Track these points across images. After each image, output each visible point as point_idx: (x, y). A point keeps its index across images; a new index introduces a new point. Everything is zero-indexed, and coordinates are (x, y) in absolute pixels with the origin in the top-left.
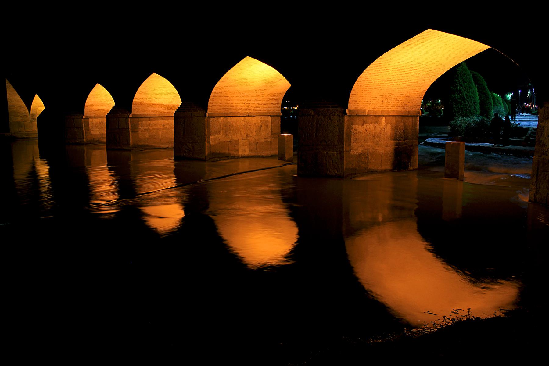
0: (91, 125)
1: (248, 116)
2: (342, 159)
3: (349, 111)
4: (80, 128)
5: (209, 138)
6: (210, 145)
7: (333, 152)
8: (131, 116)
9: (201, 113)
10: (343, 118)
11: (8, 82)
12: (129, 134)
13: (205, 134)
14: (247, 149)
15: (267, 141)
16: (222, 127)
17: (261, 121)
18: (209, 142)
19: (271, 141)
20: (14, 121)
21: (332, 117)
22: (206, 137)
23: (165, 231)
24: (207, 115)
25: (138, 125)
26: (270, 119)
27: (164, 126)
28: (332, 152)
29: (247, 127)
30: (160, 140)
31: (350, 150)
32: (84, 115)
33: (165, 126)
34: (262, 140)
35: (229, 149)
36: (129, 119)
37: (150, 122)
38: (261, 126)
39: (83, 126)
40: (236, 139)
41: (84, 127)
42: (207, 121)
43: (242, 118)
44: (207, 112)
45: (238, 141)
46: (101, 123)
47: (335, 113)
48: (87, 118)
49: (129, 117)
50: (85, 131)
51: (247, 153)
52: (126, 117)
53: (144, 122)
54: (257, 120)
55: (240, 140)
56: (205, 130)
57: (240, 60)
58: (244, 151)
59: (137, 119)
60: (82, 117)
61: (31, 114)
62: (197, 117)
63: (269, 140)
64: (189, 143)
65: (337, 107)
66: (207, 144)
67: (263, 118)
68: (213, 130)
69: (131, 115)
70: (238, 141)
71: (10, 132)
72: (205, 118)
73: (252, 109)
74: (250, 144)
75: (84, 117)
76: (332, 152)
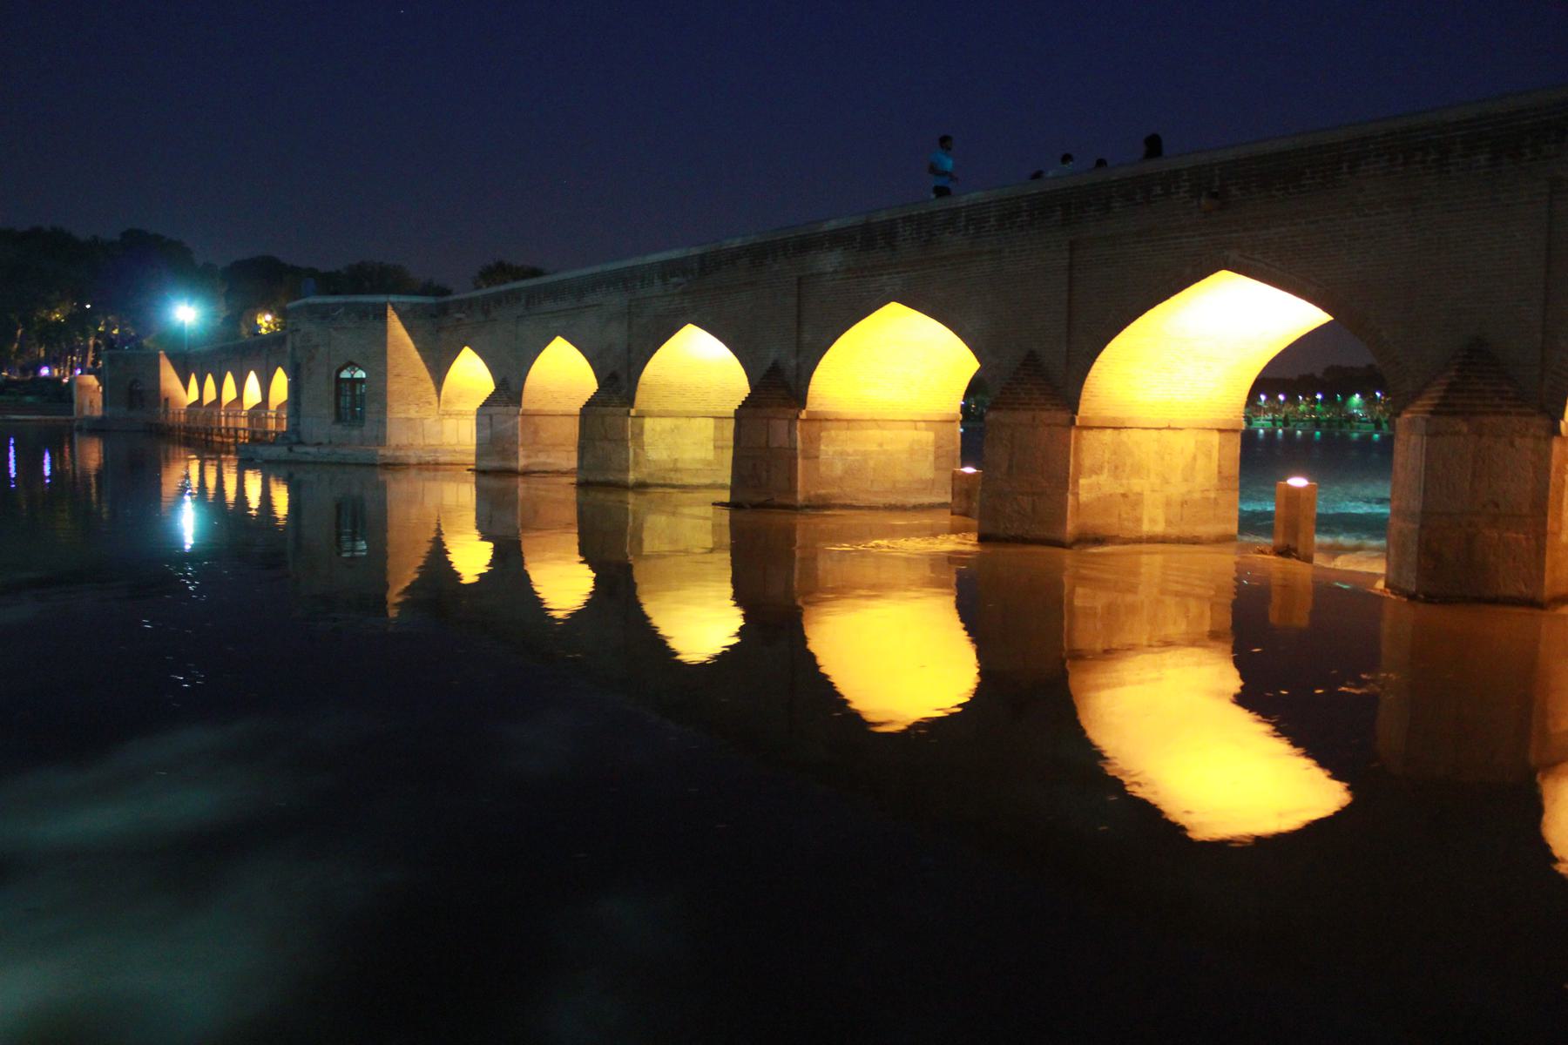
0: (647, 437)
1: (1169, 428)
2: (1540, 551)
3: (1082, 418)
4: (622, 441)
5: (1076, 482)
6: (1078, 503)
7: (1517, 533)
8: (803, 415)
9: (1062, 416)
10: (1549, 446)
11: (393, 312)
12: (796, 464)
13: (1068, 473)
14: (1161, 519)
15: (1208, 499)
16: (1107, 456)
17: (1196, 442)
18: (1076, 495)
19: (1215, 499)
20: (399, 415)
21: (1517, 442)
22: (1070, 480)
23: (1555, 800)
24: (1078, 423)
25: (820, 440)
26: (1215, 438)
27: (881, 445)
28: (1515, 535)
29: (1163, 459)
30: (869, 483)
31: (1561, 528)
32: (633, 408)
33: (885, 447)
34: (1197, 496)
35: (1120, 515)
36: (799, 424)
37: (848, 432)
38: (1195, 458)
39: (630, 436)
40: (1137, 489)
41: (632, 439)
42: (1076, 437)
43: (1154, 433)
44: (1076, 413)
45: (1141, 494)
46: (673, 431)
47: (1527, 429)
48: (641, 416)
49: (798, 417)
50: (634, 450)
51: (1159, 528)
52: (789, 417)
53: (833, 433)
54: (911, 435)
55: (1147, 493)
56: (1069, 461)
57: (1161, 302)
58: (1153, 521)
59: (818, 424)
60: (629, 412)
61: (442, 398)
62: (1049, 425)
63: (1212, 495)
64: (1022, 495)
65: (1532, 415)
66: (1070, 498)
67: (1202, 436)
68: (1087, 462)
69: (804, 412)
70: (1141, 494)
71: (387, 444)
72: (1070, 433)
73: (1178, 415)
74: (1168, 504)
75: (633, 412)
76: (1515, 535)
